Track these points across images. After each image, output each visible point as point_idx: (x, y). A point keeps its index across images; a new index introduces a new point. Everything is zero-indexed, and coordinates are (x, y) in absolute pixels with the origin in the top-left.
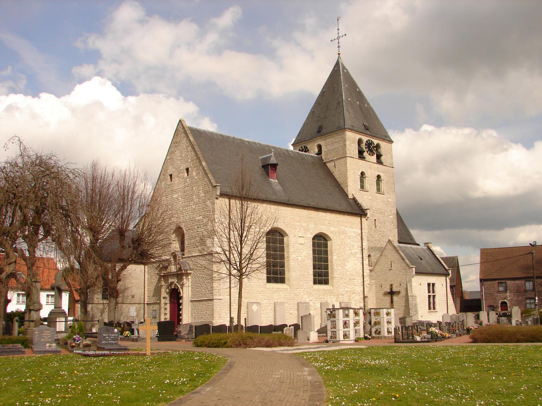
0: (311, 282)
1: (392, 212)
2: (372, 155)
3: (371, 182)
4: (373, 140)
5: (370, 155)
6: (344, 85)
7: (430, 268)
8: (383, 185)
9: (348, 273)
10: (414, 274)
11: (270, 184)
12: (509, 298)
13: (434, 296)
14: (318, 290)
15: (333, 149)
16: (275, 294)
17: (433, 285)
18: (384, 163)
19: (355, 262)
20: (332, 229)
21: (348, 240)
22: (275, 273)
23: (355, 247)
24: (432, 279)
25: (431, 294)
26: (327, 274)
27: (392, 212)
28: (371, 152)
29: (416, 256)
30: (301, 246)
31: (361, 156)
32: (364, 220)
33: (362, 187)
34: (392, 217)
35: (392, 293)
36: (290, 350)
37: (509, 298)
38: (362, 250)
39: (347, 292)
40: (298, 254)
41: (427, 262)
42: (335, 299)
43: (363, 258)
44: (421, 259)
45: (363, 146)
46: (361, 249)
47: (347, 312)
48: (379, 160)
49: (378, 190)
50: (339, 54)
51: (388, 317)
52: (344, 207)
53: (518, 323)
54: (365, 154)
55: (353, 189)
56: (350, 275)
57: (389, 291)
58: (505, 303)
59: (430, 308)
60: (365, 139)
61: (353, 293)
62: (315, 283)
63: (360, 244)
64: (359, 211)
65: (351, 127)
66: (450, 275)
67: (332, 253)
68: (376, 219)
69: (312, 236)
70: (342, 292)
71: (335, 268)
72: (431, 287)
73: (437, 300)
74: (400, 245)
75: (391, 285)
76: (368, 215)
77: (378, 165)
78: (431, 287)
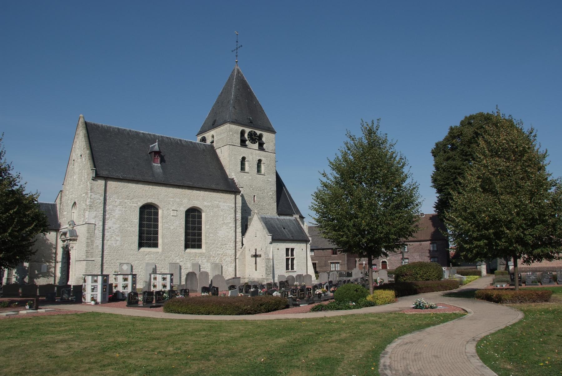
4: (256, 131)
7: (290, 236)
8: (263, 167)
11: (151, 167)
13: (293, 260)
14: (190, 253)
17: (292, 250)
19: (227, 230)
20: (205, 203)
23: (228, 218)
24: (290, 245)
28: (253, 141)
29: (279, 226)
33: (243, 169)
35: (256, 256)
41: (290, 231)
43: (236, 227)
45: (246, 136)
47: (95, 278)
49: (259, 171)
53: (525, 259)
56: (222, 240)
59: (287, 268)
60: (247, 130)
63: (233, 215)
64: (230, 188)
73: (295, 262)
74: (282, 217)
75: (256, 250)
77: (260, 151)
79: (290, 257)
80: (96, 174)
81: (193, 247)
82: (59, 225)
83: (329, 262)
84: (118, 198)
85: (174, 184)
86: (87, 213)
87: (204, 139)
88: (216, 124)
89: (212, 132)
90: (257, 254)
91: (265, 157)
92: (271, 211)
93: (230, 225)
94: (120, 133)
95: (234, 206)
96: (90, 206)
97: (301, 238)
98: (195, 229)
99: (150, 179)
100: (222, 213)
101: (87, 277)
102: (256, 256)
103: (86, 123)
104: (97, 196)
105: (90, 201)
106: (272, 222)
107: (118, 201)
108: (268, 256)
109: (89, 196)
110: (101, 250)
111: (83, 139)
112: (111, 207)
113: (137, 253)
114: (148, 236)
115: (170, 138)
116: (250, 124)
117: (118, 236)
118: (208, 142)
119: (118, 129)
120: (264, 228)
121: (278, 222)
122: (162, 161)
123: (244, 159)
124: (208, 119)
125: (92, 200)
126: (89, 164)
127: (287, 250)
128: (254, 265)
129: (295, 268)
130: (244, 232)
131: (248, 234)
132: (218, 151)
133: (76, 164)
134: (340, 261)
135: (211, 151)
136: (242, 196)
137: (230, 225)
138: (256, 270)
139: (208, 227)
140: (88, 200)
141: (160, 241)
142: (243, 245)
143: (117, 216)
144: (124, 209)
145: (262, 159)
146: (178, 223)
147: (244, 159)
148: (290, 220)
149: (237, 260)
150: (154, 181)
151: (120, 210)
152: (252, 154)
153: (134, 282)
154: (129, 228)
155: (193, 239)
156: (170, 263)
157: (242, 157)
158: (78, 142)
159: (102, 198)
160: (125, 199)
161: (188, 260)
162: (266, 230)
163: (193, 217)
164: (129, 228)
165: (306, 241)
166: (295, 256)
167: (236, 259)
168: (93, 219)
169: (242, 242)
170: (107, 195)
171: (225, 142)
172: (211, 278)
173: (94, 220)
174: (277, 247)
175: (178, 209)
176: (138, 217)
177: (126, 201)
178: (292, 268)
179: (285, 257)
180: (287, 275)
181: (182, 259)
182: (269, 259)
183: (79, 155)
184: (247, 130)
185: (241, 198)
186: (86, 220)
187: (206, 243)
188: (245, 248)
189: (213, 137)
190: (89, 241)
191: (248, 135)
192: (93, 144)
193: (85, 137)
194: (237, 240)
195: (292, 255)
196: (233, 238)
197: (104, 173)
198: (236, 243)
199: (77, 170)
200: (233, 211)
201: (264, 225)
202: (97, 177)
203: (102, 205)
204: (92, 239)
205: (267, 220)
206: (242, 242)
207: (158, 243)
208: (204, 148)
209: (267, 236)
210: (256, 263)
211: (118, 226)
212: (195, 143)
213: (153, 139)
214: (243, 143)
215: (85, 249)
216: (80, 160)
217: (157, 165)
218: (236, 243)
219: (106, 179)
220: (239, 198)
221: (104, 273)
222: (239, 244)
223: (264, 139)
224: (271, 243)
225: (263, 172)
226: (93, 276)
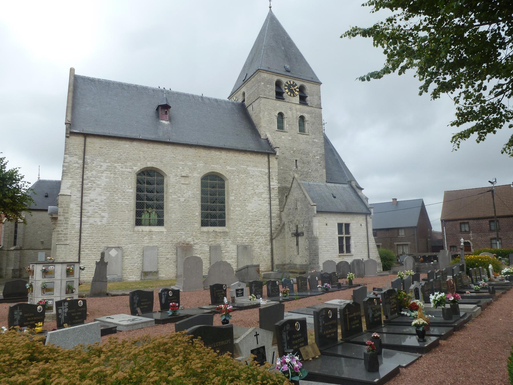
0: (198, 225)
2: (294, 96)
4: (296, 82)
5: (290, 95)
9: (249, 214)
10: (315, 212)
12: (472, 239)
13: (348, 239)
16: (145, 238)
17: (347, 226)
18: (309, 104)
19: (260, 202)
20: (228, 168)
21: (250, 179)
23: (261, 187)
24: (344, 220)
25: (344, 235)
26: (223, 216)
27: (319, 152)
30: (185, 186)
32: (272, 159)
34: (319, 157)
37: (472, 239)
38: (270, 190)
39: (248, 234)
40: (179, 195)
44: (335, 197)
46: (268, 189)
48: (303, 99)
50: (270, 7)
51: (46, 280)
52: (252, 145)
55: (267, 129)
58: (468, 243)
59: (341, 250)
61: (256, 235)
62: (204, 224)
63: (267, 184)
64: (267, 151)
65: (267, 69)
67: (228, 193)
68: (297, 159)
69: (202, 174)
70: (241, 235)
71: (232, 208)
73: (352, 242)
74: (329, 184)
75: (297, 226)
76: (277, 154)
78: (344, 229)
83: (396, 243)
84: (105, 162)
91: (308, 113)
95: (267, 171)
100: (252, 180)
102: (297, 235)
104: (75, 159)
107: (105, 166)
110: (78, 230)
117: (104, 211)
127: (340, 225)
134: (409, 243)
145: (305, 115)
146: (190, 193)
151: (106, 177)
152: (291, 109)
154: (120, 201)
157: (278, 112)
160: (115, 162)
161: (202, 241)
164: (120, 201)
168: (68, 188)
173: (70, 191)
177: (116, 165)
179: (336, 235)
180: (337, 260)
189: (244, 94)
195: (348, 232)
200: (266, 177)
203: (80, 171)
211: (105, 198)
214: (279, 95)
220: (274, 162)
224: (72, 70)
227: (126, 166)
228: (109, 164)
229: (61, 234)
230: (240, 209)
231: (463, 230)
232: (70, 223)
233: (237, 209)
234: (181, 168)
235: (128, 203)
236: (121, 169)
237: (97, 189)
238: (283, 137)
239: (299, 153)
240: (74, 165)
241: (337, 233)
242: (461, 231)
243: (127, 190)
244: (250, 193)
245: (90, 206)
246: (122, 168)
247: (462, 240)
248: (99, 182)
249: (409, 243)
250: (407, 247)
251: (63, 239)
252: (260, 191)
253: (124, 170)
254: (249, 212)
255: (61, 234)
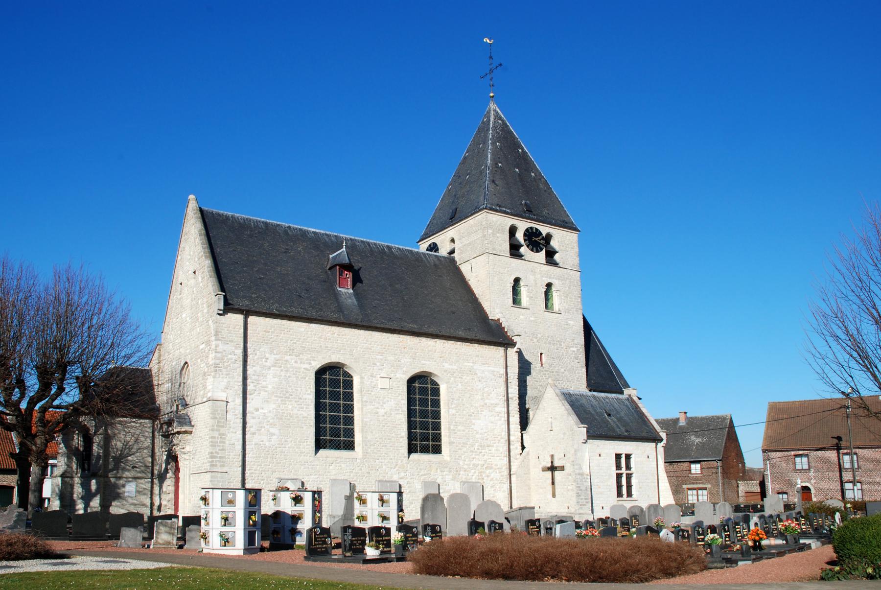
1: (576, 342)
3: (530, 294)
5: (532, 250)
6: (493, 144)
7: (623, 430)
9: (477, 436)
11: (336, 295)
13: (629, 477)
15: (470, 244)
17: (628, 457)
18: (560, 265)
20: (447, 366)
22: (425, 438)
27: (576, 342)
29: (598, 410)
31: (515, 252)
33: (516, 301)
34: (575, 349)
35: (552, 469)
36: (10, 567)
37: (812, 481)
41: (620, 419)
42: (451, 477)
45: (520, 236)
54: (524, 250)
57: (549, 465)
59: (619, 494)
60: (523, 225)
63: (502, 390)
64: (496, 336)
66: (664, 441)
72: (622, 461)
73: (634, 481)
75: (552, 456)
78: (622, 461)
79: (624, 470)
80: (226, 303)
81: (425, 450)
82: (158, 410)
84: (271, 353)
85: (382, 326)
86: (210, 379)
87: (434, 247)
88: (457, 216)
89: (451, 232)
90: (556, 464)
92: (579, 384)
93: (498, 409)
94: (267, 229)
95: (503, 371)
96: (216, 366)
97: (644, 434)
98: (426, 417)
99: (334, 316)
101: (210, 496)
103: (201, 211)
104: (229, 348)
105: (216, 358)
106: (584, 401)
107: (272, 358)
108: (581, 468)
109: (213, 347)
111: (198, 240)
112: (257, 368)
113: (312, 459)
114: (333, 427)
115: (368, 243)
116: (527, 213)
117: (273, 425)
118: (443, 252)
119: (266, 224)
120: (569, 414)
121: (595, 403)
122: (357, 280)
123: (517, 281)
124: (440, 208)
125: (219, 355)
126: (210, 284)
127: (618, 456)
128: (550, 486)
129: (634, 492)
130: (524, 423)
131: (531, 428)
132: (465, 269)
133: (186, 291)
135: (450, 265)
136: (520, 353)
137: (498, 409)
138: (554, 496)
139: (454, 411)
140: (212, 355)
141: (358, 438)
142: (523, 448)
143: (270, 387)
144: (283, 374)
147: (517, 281)
148: (617, 399)
149: (513, 478)
150: (342, 320)
152: (533, 272)
153: (317, 508)
154: (295, 411)
155: (424, 434)
156: (380, 481)
158: (187, 248)
159: (240, 352)
161: (418, 475)
162: (575, 417)
163: (422, 394)
165: (657, 440)
166: (633, 470)
167: (510, 475)
169: (522, 443)
170: (248, 345)
171: (479, 247)
172: (473, 507)
174: (598, 451)
175: (392, 376)
176: (313, 390)
177: (287, 358)
178: (629, 494)
179: (614, 471)
181: (402, 474)
182: (582, 474)
183: (191, 272)
184: (523, 225)
185: (516, 357)
186: (209, 395)
187: (451, 443)
188: (528, 454)
189: (453, 241)
190: (216, 434)
191: (525, 235)
192: (218, 250)
193: (200, 235)
194: (512, 438)
195: (628, 467)
196: (504, 434)
197: (244, 303)
198: (509, 444)
199: (187, 302)
201: (568, 407)
202: (228, 307)
204: (222, 430)
205: (573, 398)
206: (522, 443)
207: (353, 442)
208: (437, 262)
209: (575, 428)
210: (553, 483)
211: (274, 406)
212: (418, 253)
213: (336, 244)
214: (515, 250)
215: (208, 450)
216: (192, 282)
217: (346, 291)
218: (509, 444)
219: (247, 313)
220: (512, 353)
221: (248, 486)
222: (516, 447)
223: (554, 243)
225: (556, 307)
226: (225, 490)
227: (301, 359)
228: (277, 357)
229: (216, 457)
230: (462, 428)
231: (799, 467)
232: (227, 442)
233: (459, 428)
234: (378, 364)
235: (306, 415)
236: (295, 365)
237: (262, 393)
238: (522, 317)
239: (545, 343)
240: (230, 356)
241: (614, 468)
242: (795, 469)
243: (305, 396)
244: (477, 405)
245: (254, 418)
246: (296, 362)
247: (799, 481)
248: (264, 383)
249: (708, 486)
250: (705, 492)
251: (219, 464)
252: (492, 402)
253: (298, 365)
254: (477, 433)
255: (216, 457)
